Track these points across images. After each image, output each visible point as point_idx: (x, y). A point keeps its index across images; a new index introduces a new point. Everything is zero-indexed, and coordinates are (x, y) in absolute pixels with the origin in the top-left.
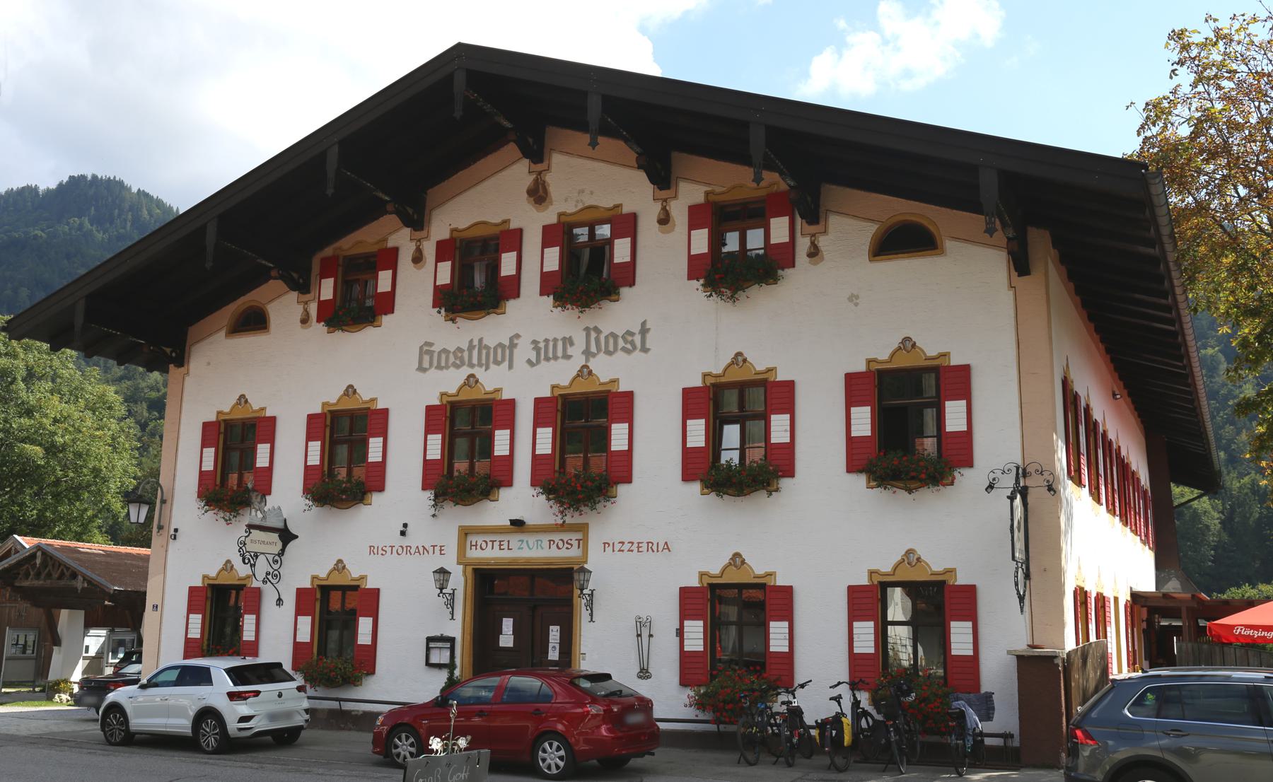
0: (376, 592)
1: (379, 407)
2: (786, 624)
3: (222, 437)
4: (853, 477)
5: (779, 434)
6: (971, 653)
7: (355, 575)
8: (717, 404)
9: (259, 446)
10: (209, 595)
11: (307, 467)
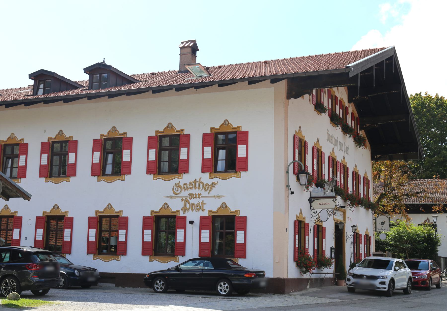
0: (127, 218)
1: (74, 139)
4: (93, 177)
5: (22, 162)
7: (13, 211)
10: (154, 220)
11: (148, 162)
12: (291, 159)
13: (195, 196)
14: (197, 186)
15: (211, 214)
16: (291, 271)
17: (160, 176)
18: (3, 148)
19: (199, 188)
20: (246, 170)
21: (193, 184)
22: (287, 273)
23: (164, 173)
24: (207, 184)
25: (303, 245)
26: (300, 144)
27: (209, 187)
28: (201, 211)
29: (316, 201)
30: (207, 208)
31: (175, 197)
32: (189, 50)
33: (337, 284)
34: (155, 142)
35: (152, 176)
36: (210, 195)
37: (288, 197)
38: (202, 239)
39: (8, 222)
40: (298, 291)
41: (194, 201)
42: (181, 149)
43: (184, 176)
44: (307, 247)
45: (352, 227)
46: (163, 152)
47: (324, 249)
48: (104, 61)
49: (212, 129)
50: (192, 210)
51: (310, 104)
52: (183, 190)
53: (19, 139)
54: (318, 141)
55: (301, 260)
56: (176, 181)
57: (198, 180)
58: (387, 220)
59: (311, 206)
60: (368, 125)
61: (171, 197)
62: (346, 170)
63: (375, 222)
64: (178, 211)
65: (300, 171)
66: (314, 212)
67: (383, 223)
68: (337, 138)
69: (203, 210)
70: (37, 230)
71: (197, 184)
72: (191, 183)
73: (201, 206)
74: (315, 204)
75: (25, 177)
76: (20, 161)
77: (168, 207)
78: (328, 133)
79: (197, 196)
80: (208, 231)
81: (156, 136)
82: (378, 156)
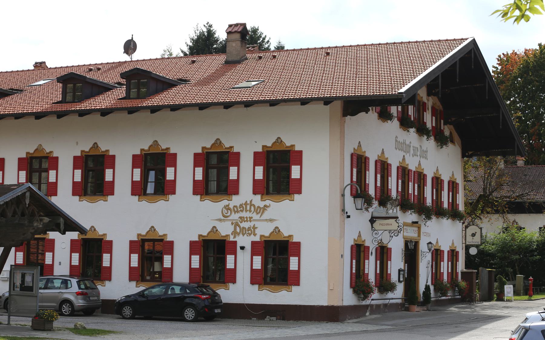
1: (54, 155)
2: (51, 253)
3: (143, 162)
4: (134, 197)
5: (52, 179)
6: (233, 267)
8: (31, 164)
9: (107, 170)
12: (348, 181)
13: (245, 219)
14: (248, 208)
15: (263, 239)
16: (348, 298)
17: (207, 197)
18: (29, 161)
19: (250, 211)
20: (299, 192)
21: (244, 206)
22: (343, 300)
23: (213, 194)
24: (259, 207)
25: (362, 268)
26: (359, 162)
27: (261, 210)
28: (252, 235)
29: (378, 222)
30: (259, 232)
31: (224, 220)
32: (238, 36)
33: (407, 309)
34: (201, 159)
35: (199, 197)
36: (262, 218)
37: (344, 221)
38: (254, 265)
39: (38, 245)
40: (355, 318)
42: (231, 168)
43: (234, 197)
44: (366, 272)
45: (428, 244)
46: (210, 170)
47: (389, 272)
48: (132, 38)
49: (264, 147)
50: (243, 235)
51: (373, 113)
52: (233, 213)
53: (48, 151)
54: (383, 152)
55: (360, 285)
56: (225, 202)
57: (249, 202)
58: (478, 231)
59: (372, 227)
61: (220, 220)
62: (421, 177)
64: (227, 236)
65: (359, 192)
67: (473, 235)
68: (410, 142)
69: (255, 235)
70: (73, 254)
71: (248, 207)
72: (241, 205)
73: (252, 231)
74: (377, 225)
75: (56, 195)
76: (50, 176)
77: (217, 230)
78: (396, 141)
79: (248, 219)
80: (260, 257)
81: (203, 153)
82: (470, 153)
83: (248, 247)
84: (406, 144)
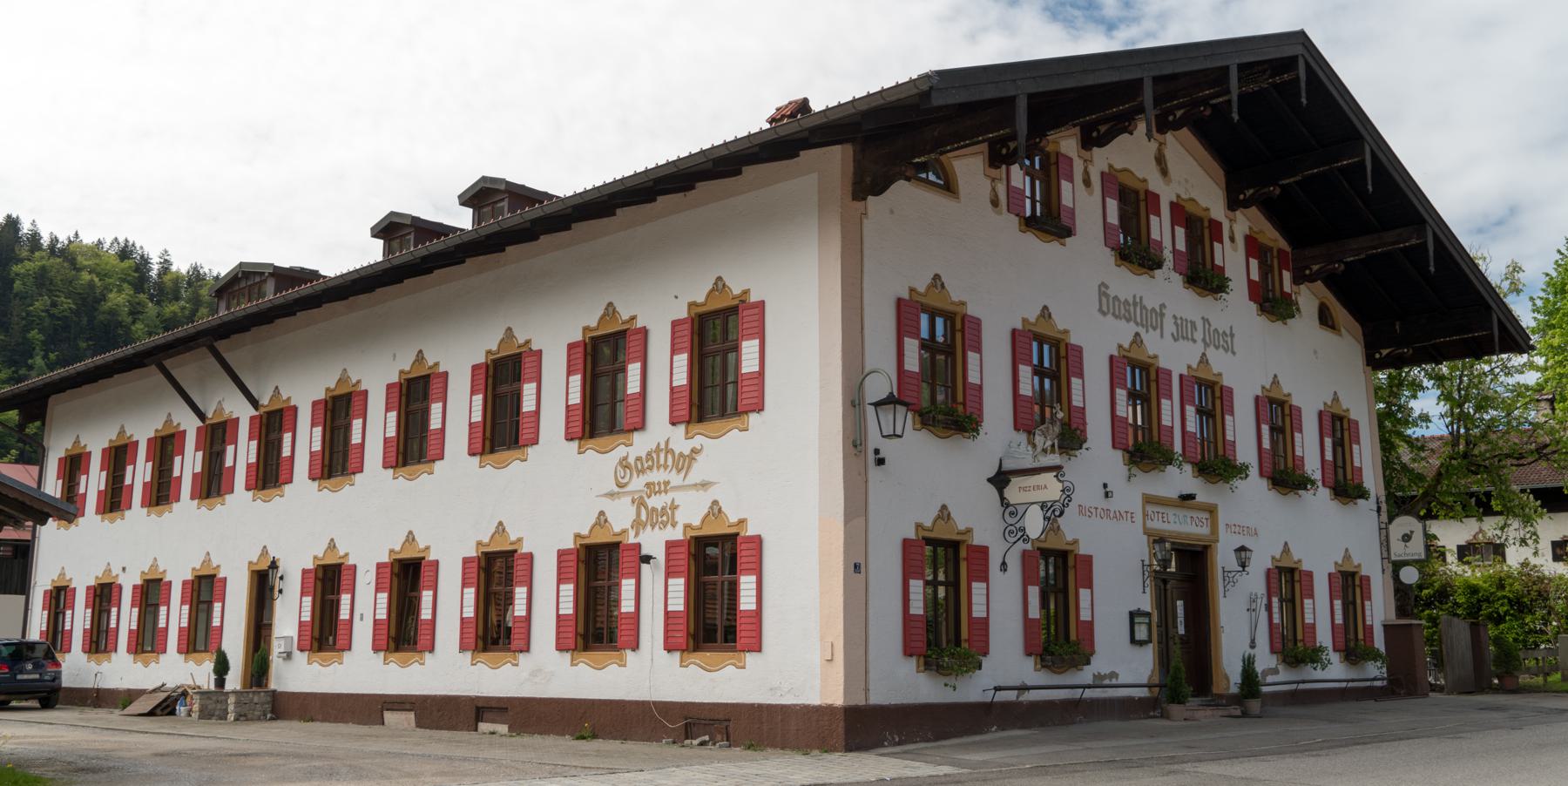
19: (666, 467)
24: (681, 455)
27: (685, 462)
29: (1016, 482)
30: (682, 517)
36: (687, 482)
41: (656, 502)
56: (621, 451)
57: (663, 446)
59: (1002, 498)
60: (1315, 268)
61: (611, 495)
63: (1387, 536)
64: (624, 531)
66: (1011, 514)
67: (1407, 538)
69: (674, 525)
73: (665, 516)
74: (1013, 493)
83: (659, 553)
84: (1143, 307)
